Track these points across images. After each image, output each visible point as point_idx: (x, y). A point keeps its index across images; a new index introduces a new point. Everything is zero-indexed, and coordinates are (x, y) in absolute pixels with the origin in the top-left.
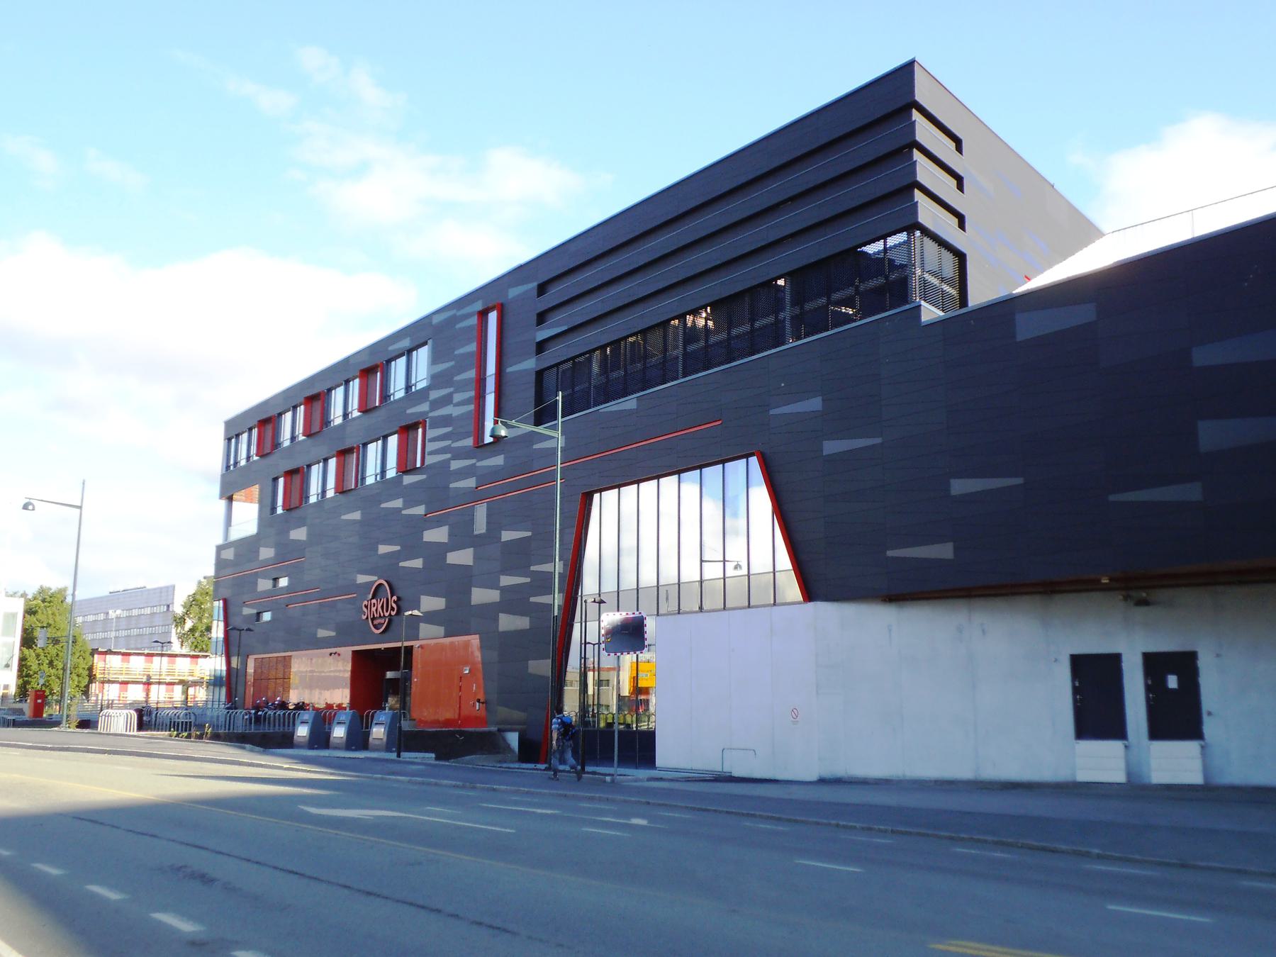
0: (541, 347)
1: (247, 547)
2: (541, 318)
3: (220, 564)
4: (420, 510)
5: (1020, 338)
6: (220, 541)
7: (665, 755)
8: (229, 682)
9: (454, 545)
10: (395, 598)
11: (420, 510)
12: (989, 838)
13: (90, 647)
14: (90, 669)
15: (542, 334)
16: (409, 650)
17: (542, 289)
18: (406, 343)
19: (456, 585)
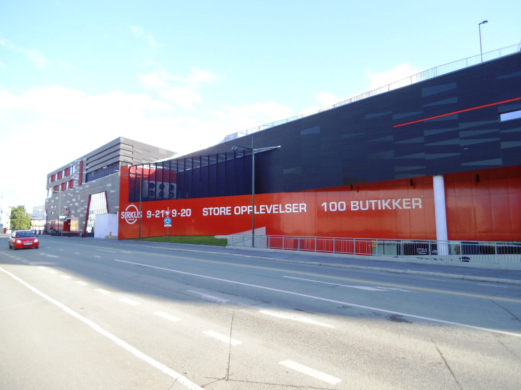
0: (87, 170)
1: (50, 200)
2: (87, 165)
3: (46, 203)
4: (72, 195)
5: (264, 228)
6: (46, 198)
7: (96, 236)
8: (46, 226)
9: (76, 202)
10: (168, 224)
11: (72, 195)
12: (494, 244)
13: (30, 218)
14: (31, 223)
15: (87, 167)
16: (399, 253)
17: (87, 160)
18: (71, 165)
19: (76, 208)
